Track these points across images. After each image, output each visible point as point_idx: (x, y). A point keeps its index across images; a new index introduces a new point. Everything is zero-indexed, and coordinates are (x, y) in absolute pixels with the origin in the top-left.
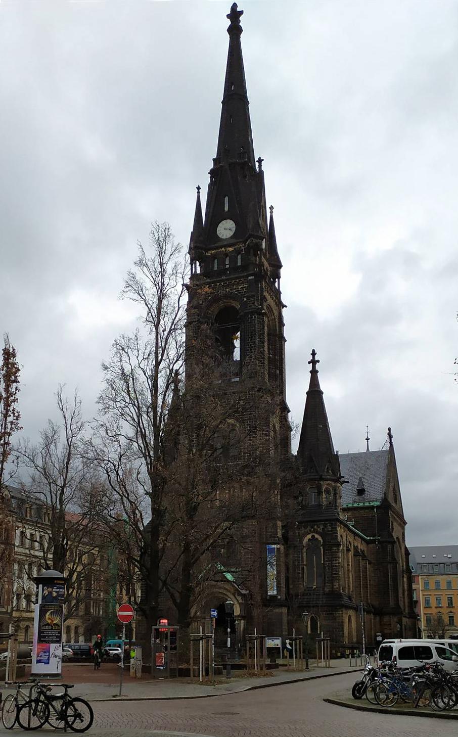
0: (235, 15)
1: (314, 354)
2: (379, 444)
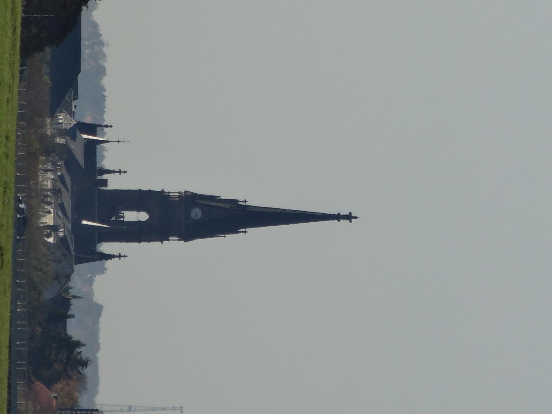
0: (349, 217)
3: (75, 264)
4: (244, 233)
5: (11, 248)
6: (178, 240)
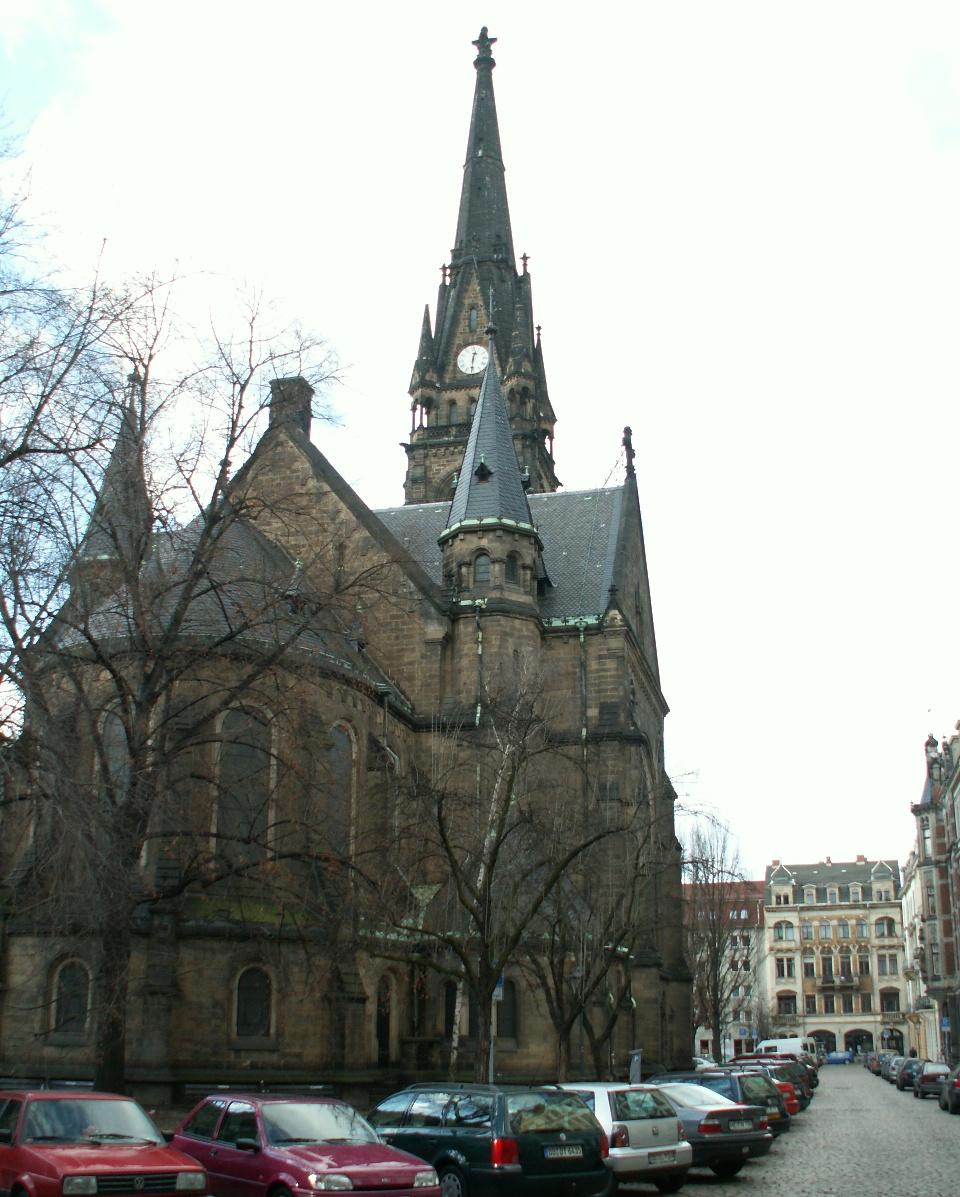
0: (484, 42)
3: (555, 483)
4: (528, 261)
5: (556, 1156)
6: (551, 438)
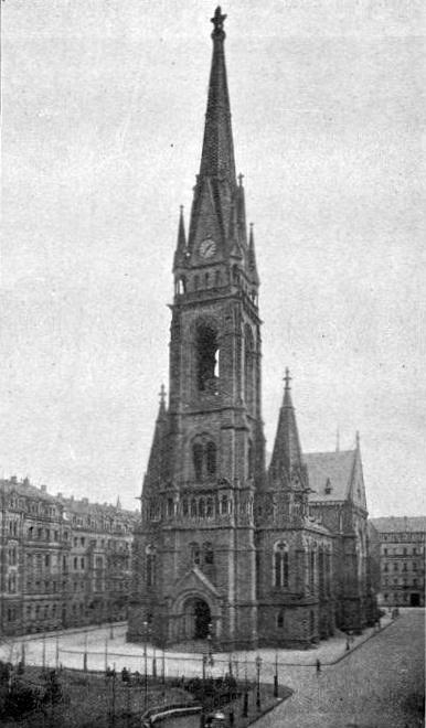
0: (218, 19)
1: (287, 372)
2: (347, 444)
